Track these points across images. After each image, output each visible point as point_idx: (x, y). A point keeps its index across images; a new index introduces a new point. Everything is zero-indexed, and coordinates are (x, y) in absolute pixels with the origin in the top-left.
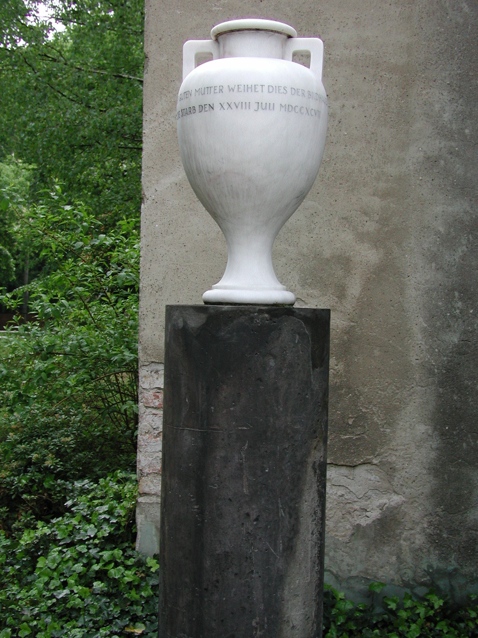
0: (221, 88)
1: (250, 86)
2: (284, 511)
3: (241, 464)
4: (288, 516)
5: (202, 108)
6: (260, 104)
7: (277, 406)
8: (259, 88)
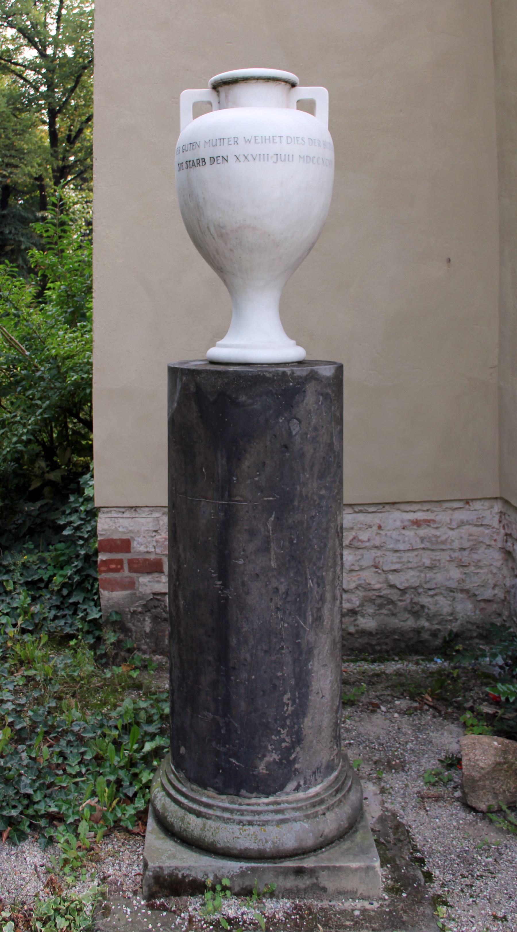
0: (236, 139)
1: (267, 137)
2: (312, 582)
3: (268, 537)
4: (316, 586)
5: (213, 160)
6: (279, 156)
7: (303, 473)
8: (277, 140)
